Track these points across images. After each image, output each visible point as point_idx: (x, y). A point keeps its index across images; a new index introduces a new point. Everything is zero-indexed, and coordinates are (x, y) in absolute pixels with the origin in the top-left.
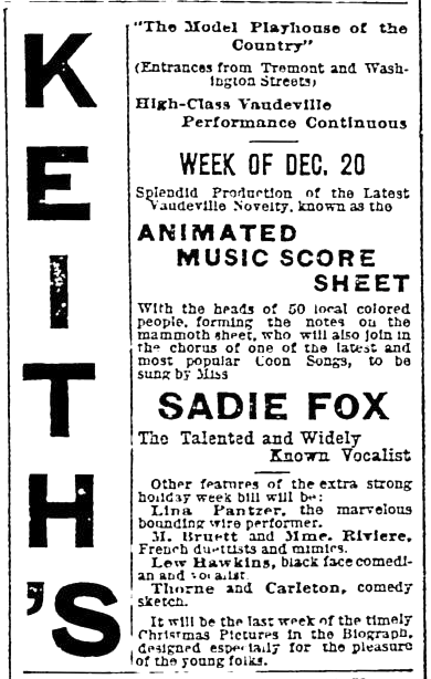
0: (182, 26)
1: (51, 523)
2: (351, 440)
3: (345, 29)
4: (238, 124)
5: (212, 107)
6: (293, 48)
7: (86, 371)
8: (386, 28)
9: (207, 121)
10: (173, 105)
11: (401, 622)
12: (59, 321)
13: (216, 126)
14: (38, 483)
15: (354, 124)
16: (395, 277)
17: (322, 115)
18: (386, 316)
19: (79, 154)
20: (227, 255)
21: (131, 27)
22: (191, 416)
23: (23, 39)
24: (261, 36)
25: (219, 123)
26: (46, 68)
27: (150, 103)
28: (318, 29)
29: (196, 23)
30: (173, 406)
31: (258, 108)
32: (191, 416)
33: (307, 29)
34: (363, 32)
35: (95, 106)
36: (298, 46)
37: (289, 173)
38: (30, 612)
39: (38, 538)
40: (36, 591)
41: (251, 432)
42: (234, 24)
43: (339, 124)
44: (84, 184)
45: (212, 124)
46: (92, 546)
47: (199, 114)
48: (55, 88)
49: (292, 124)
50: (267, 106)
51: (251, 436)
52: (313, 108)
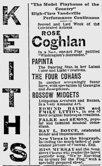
0: (43, 4)
2: (84, 82)
3: (84, 5)
4: (57, 18)
5: (51, 14)
6: (71, 9)
7: (19, 91)
8: (94, 4)
9: (50, 18)
10: (41, 14)
12: (12, 64)
13: (52, 19)
14: (6, 118)
15: (86, 18)
17: (78, 16)
19: (17, 36)
20: (54, 33)
21: (30, 5)
23: (4, 117)
24: (63, 7)
25: (52, 18)
26: (9, 14)
27: (35, 14)
28: (77, 5)
29: (47, 4)
31: (62, 14)
33: (74, 5)
34: (89, 25)
36: (72, 9)
38: (4, 150)
39: (6, 132)
40: (6, 145)
42: (56, 4)
43: (82, 18)
44: (18, 44)
45: (51, 18)
46: (20, 134)
47: (47, 16)
48: (10, 21)
49: (71, 18)
50: (64, 14)
52: (76, 14)
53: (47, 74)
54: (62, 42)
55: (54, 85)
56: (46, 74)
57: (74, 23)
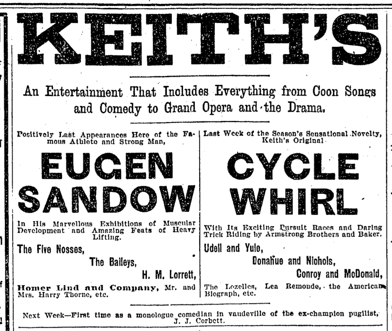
1: (189, 25)
11: (48, 136)
16: (136, 96)
18: (37, 292)
22: (46, 210)
30: (29, 199)
32: (46, 210)
35: (280, 154)
37: (254, 264)
41: (351, 226)
46: (58, 164)
51: (354, 234)
53: (40, 245)
54: (112, 224)
55: (322, 233)
56: (46, 157)
57: (46, 314)
